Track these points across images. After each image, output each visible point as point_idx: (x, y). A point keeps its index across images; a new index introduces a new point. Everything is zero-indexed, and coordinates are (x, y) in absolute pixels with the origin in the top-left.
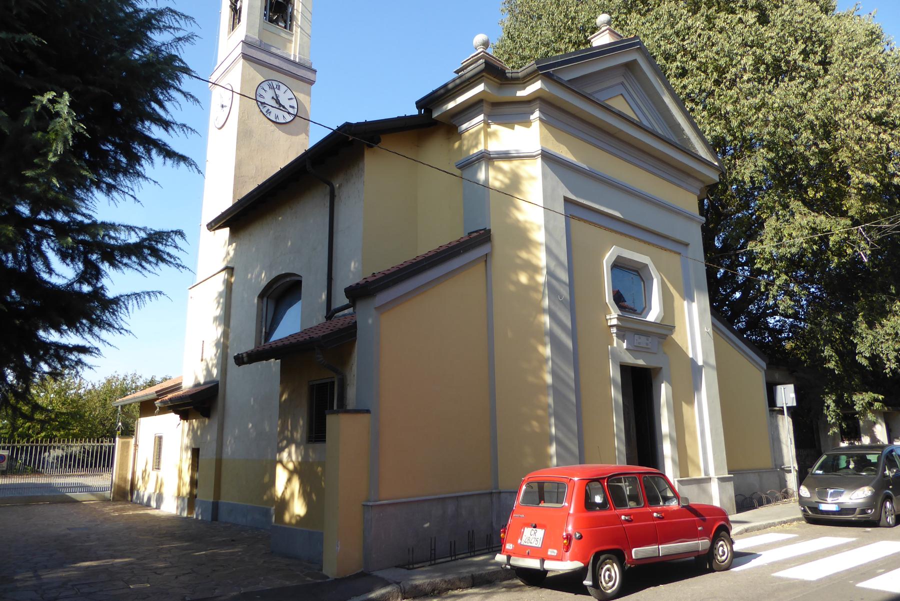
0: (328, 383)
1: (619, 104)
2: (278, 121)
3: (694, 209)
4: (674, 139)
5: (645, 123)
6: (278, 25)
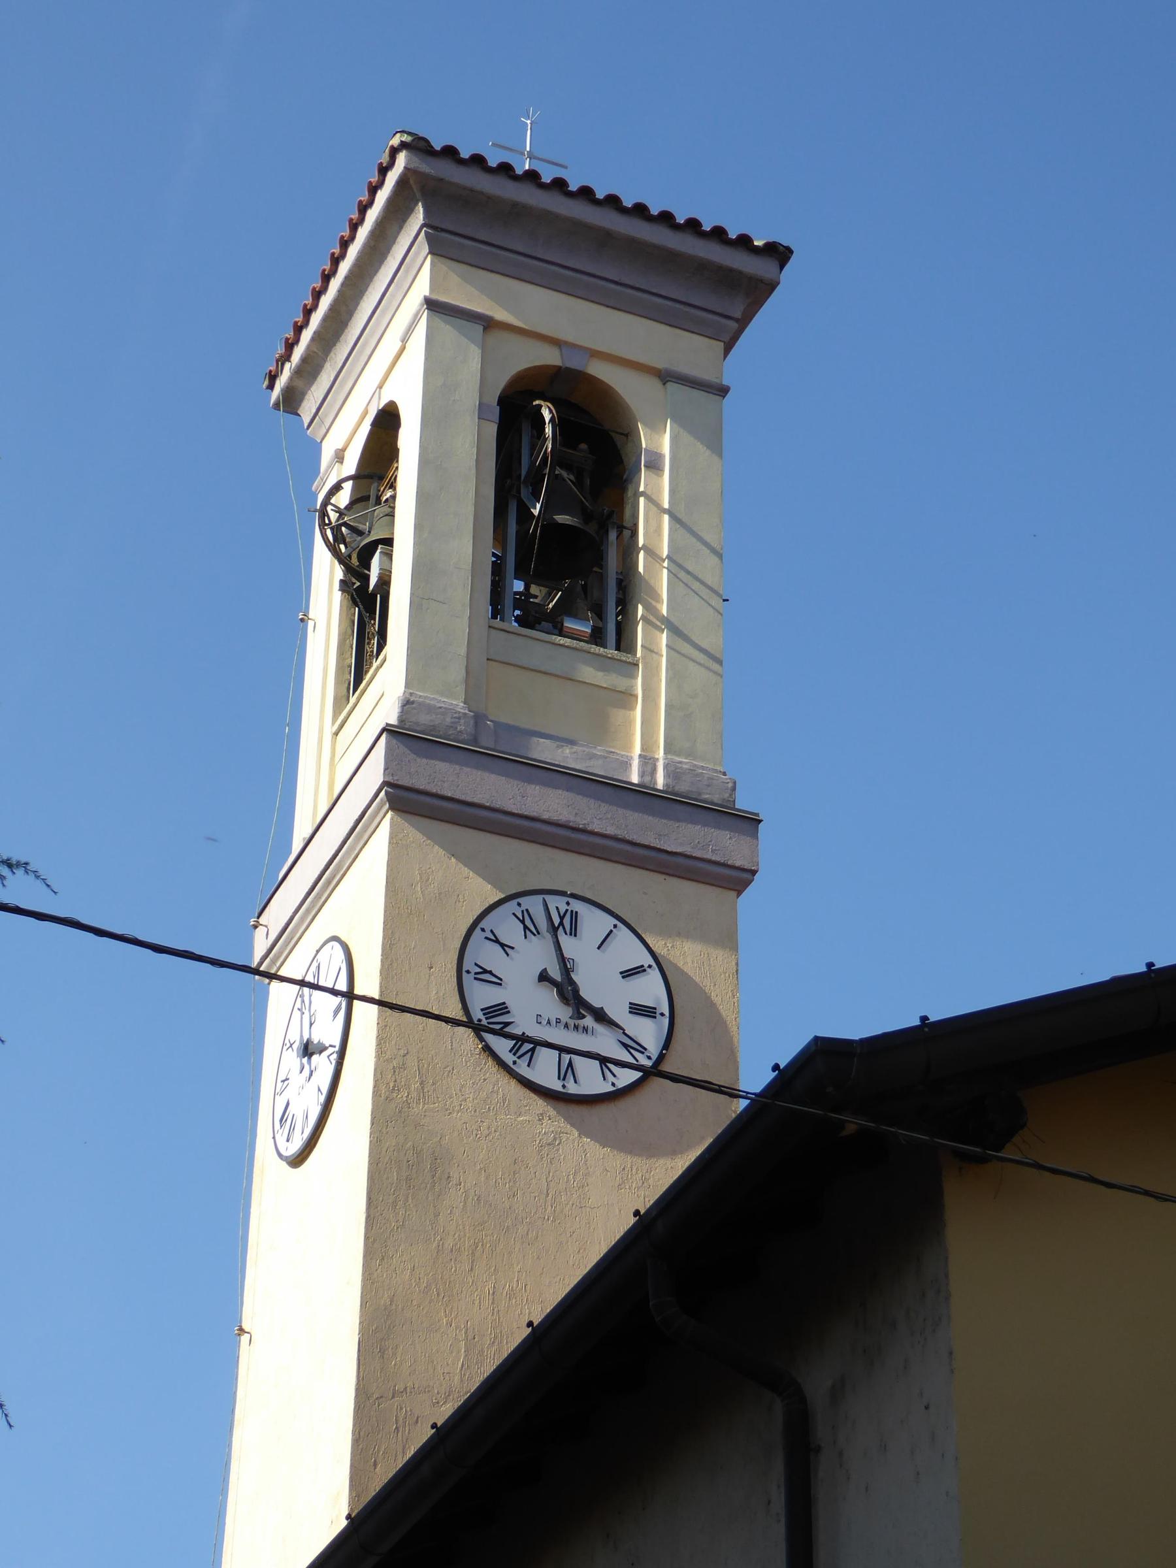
2: (572, 1088)
6: (561, 632)
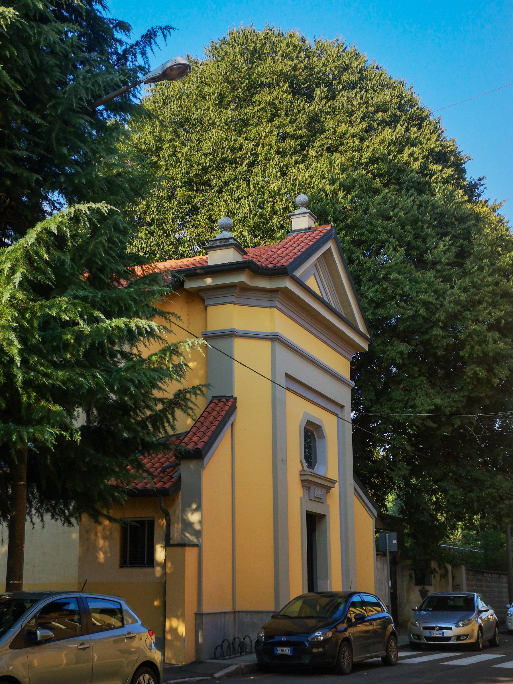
0: (145, 521)
1: (312, 283)
3: (346, 375)
4: (342, 313)
5: (326, 299)
